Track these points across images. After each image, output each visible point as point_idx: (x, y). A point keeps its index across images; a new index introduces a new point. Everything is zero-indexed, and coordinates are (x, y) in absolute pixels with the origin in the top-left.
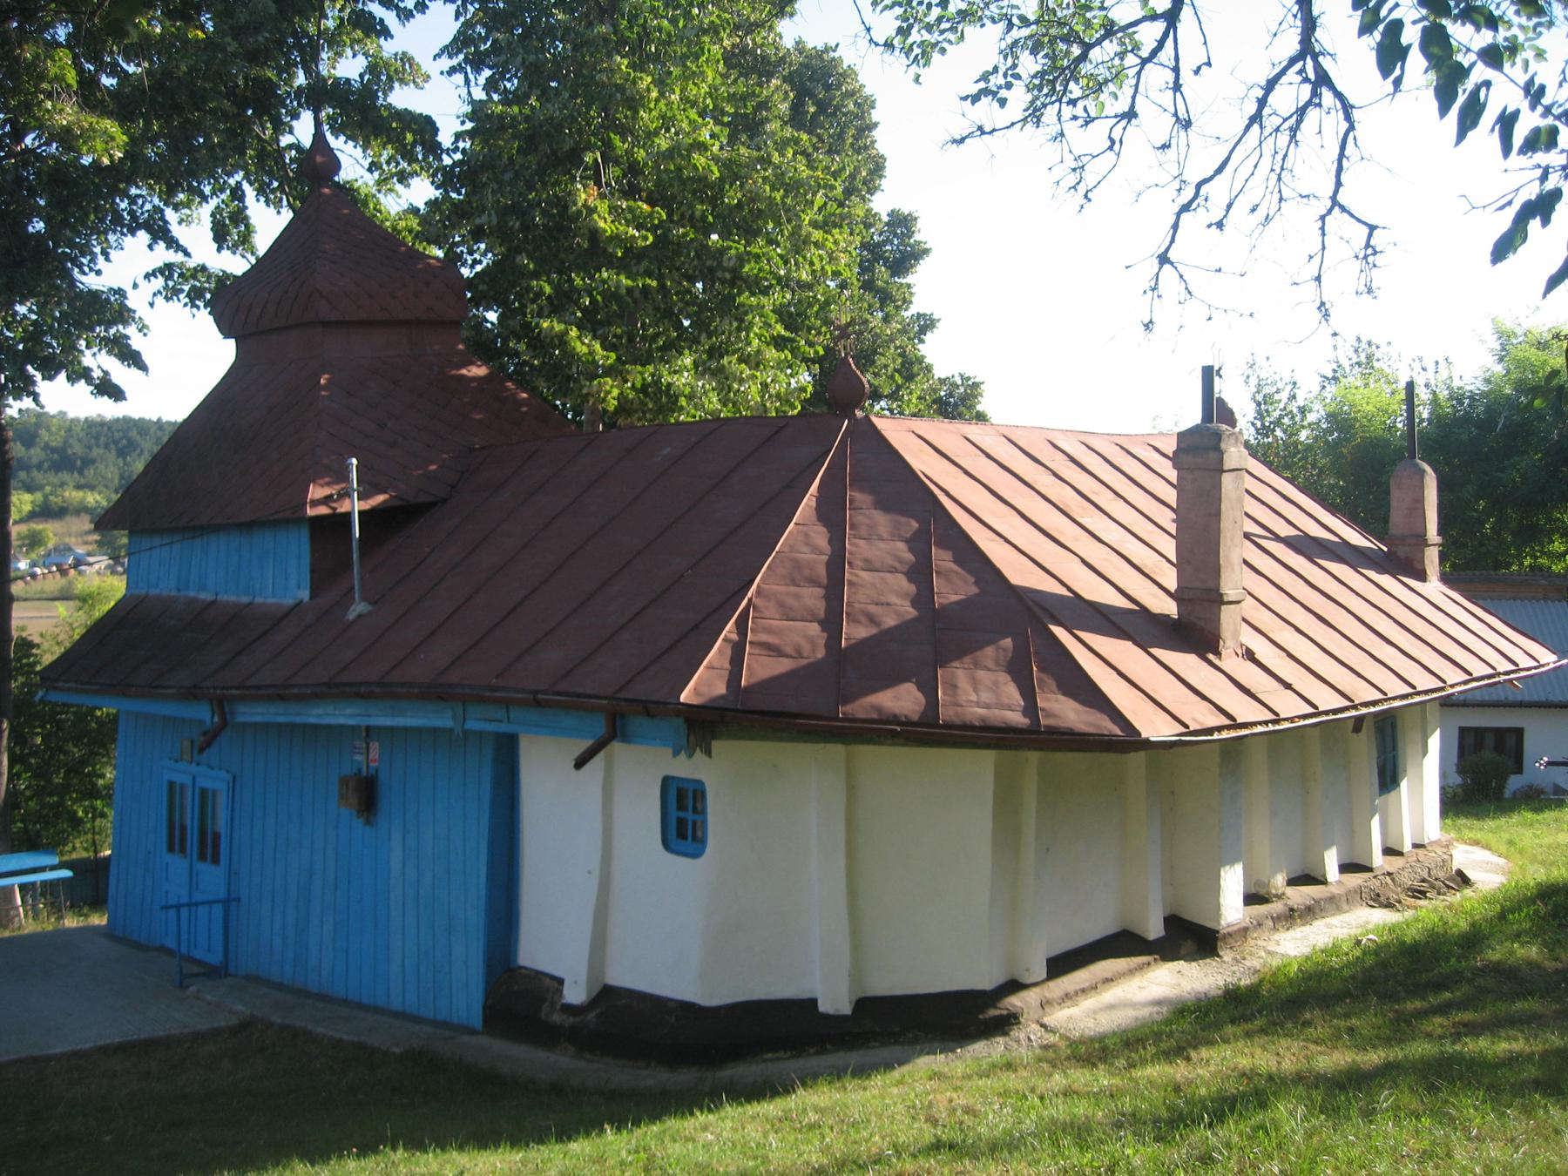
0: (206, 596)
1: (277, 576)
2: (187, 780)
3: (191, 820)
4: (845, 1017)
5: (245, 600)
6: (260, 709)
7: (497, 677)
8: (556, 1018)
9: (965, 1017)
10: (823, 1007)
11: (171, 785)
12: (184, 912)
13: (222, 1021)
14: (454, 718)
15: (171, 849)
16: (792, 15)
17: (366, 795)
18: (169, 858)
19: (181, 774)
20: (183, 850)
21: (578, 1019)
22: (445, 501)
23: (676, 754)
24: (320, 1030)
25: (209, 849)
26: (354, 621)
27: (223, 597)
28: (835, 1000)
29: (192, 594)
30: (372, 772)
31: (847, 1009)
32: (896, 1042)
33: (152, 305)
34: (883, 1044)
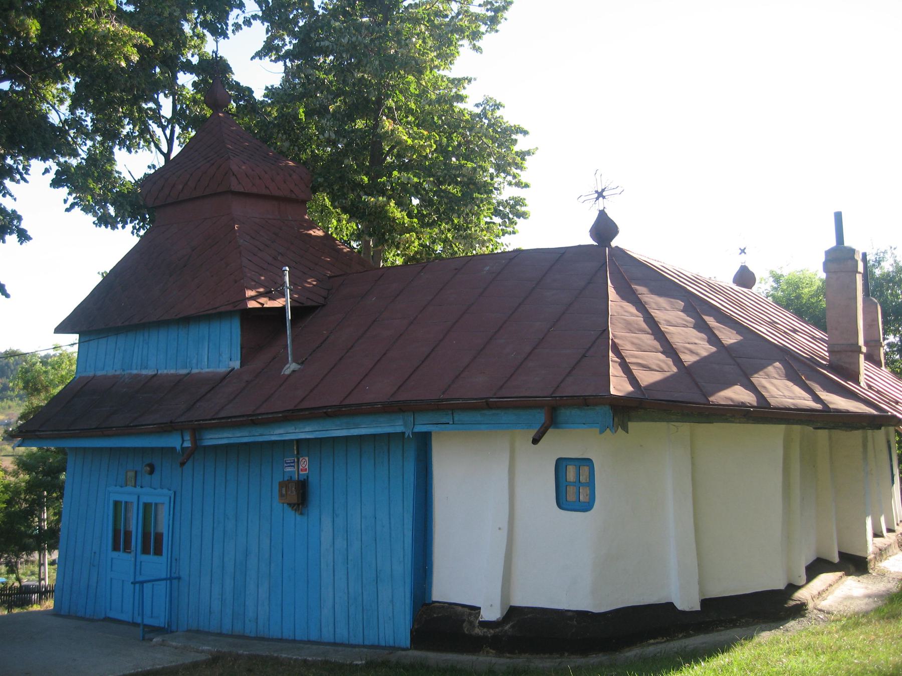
0: (150, 372)
1: (215, 352)
2: (133, 499)
3: (135, 526)
4: (697, 612)
5: (183, 372)
6: (225, 435)
7: (443, 393)
8: (478, 631)
9: (773, 608)
10: (680, 606)
11: (117, 504)
12: (148, 587)
14: (405, 425)
15: (116, 548)
16: (497, 31)
17: (300, 495)
18: (115, 554)
19: (127, 494)
20: (127, 548)
21: (497, 630)
22: (324, 305)
23: (601, 432)
24: (284, 656)
25: (153, 544)
26: (289, 375)
27: (163, 371)
28: (687, 600)
29: (135, 372)
30: (302, 478)
31: (698, 608)
32: (735, 626)
34: (727, 628)
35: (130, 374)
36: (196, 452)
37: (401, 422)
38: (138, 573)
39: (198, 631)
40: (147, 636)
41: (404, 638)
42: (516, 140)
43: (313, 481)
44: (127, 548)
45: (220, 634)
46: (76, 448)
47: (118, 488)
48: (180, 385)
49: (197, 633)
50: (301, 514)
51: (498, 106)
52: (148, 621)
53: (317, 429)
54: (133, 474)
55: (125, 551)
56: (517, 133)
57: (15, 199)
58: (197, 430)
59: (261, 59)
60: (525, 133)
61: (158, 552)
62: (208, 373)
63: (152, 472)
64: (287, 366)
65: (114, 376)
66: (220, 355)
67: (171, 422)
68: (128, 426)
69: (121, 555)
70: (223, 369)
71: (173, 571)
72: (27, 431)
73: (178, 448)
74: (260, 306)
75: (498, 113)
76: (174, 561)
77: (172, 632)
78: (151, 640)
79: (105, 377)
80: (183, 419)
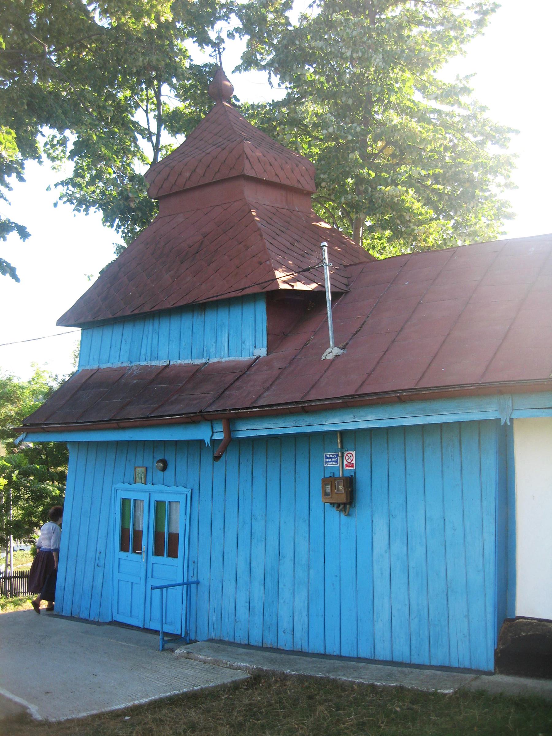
0: (162, 363)
1: (237, 339)
3: (145, 524)
6: (266, 425)
11: (124, 501)
13: (241, 676)
15: (124, 548)
17: (346, 495)
18: (124, 554)
19: (140, 493)
20: (137, 549)
25: (167, 544)
26: (333, 361)
29: (143, 363)
30: (347, 475)
33: (55, 205)
35: (139, 365)
36: (232, 444)
37: (494, 407)
38: (149, 575)
39: (221, 641)
40: (167, 646)
41: (485, 658)
42: (509, 139)
43: (362, 479)
44: (137, 549)
45: (248, 646)
46: (79, 443)
47: (126, 486)
48: (198, 375)
49: (219, 643)
50: (348, 515)
51: (483, 109)
52: (168, 629)
53: (382, 416)
54: (143, 470)
55: (134, 551)
56: (508, 132)
57: (10, 204)
58: (231, 419)
59: (240, 72)
60: (517, 132)
61: (173, 553)
62: (229, 361)
63: (164, 469)
64: (329, 350)
65: (121, 369)
66: (242, 342)
67: (201, 412)
68: (148, 417)
69: (130, 555)
70: (246, 357)
71: (191, 574)
72: (31, 425)
73: (207, 441)
74: (290, 288)
75: (485, 115)
76: (191, 564)
77: (191, 642)
78: (172, 650)
79: (111, 370)
80: (213, 408)
